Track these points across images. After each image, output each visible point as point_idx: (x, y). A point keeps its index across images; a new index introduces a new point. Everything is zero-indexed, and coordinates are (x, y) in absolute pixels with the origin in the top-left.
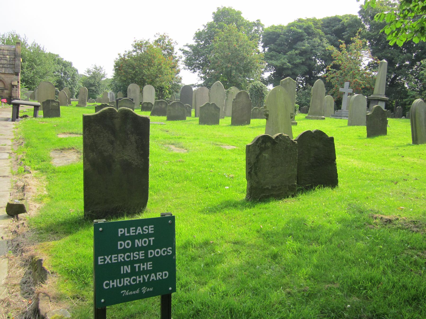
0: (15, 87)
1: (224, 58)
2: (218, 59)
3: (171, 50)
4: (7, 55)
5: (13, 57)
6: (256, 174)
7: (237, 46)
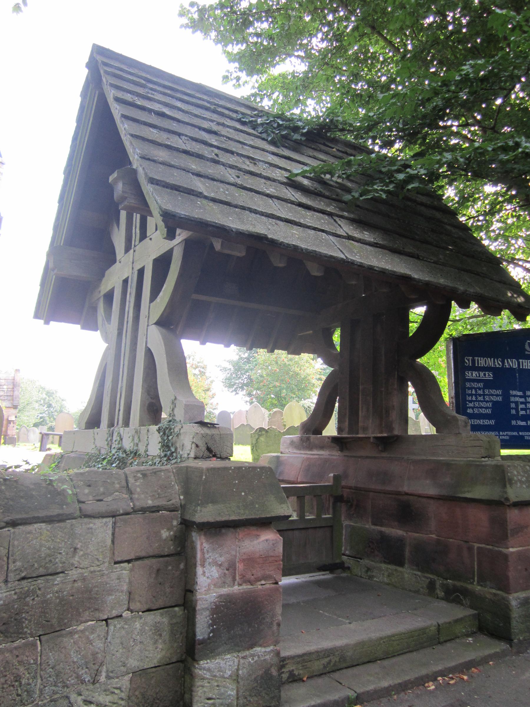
0: (12, 423)
1: (270, 375)
2: (264, 377)
3: (203, 368)
4: (4, 385)
5: (11, 387)
6: (257, 450)
7: (286, 360)
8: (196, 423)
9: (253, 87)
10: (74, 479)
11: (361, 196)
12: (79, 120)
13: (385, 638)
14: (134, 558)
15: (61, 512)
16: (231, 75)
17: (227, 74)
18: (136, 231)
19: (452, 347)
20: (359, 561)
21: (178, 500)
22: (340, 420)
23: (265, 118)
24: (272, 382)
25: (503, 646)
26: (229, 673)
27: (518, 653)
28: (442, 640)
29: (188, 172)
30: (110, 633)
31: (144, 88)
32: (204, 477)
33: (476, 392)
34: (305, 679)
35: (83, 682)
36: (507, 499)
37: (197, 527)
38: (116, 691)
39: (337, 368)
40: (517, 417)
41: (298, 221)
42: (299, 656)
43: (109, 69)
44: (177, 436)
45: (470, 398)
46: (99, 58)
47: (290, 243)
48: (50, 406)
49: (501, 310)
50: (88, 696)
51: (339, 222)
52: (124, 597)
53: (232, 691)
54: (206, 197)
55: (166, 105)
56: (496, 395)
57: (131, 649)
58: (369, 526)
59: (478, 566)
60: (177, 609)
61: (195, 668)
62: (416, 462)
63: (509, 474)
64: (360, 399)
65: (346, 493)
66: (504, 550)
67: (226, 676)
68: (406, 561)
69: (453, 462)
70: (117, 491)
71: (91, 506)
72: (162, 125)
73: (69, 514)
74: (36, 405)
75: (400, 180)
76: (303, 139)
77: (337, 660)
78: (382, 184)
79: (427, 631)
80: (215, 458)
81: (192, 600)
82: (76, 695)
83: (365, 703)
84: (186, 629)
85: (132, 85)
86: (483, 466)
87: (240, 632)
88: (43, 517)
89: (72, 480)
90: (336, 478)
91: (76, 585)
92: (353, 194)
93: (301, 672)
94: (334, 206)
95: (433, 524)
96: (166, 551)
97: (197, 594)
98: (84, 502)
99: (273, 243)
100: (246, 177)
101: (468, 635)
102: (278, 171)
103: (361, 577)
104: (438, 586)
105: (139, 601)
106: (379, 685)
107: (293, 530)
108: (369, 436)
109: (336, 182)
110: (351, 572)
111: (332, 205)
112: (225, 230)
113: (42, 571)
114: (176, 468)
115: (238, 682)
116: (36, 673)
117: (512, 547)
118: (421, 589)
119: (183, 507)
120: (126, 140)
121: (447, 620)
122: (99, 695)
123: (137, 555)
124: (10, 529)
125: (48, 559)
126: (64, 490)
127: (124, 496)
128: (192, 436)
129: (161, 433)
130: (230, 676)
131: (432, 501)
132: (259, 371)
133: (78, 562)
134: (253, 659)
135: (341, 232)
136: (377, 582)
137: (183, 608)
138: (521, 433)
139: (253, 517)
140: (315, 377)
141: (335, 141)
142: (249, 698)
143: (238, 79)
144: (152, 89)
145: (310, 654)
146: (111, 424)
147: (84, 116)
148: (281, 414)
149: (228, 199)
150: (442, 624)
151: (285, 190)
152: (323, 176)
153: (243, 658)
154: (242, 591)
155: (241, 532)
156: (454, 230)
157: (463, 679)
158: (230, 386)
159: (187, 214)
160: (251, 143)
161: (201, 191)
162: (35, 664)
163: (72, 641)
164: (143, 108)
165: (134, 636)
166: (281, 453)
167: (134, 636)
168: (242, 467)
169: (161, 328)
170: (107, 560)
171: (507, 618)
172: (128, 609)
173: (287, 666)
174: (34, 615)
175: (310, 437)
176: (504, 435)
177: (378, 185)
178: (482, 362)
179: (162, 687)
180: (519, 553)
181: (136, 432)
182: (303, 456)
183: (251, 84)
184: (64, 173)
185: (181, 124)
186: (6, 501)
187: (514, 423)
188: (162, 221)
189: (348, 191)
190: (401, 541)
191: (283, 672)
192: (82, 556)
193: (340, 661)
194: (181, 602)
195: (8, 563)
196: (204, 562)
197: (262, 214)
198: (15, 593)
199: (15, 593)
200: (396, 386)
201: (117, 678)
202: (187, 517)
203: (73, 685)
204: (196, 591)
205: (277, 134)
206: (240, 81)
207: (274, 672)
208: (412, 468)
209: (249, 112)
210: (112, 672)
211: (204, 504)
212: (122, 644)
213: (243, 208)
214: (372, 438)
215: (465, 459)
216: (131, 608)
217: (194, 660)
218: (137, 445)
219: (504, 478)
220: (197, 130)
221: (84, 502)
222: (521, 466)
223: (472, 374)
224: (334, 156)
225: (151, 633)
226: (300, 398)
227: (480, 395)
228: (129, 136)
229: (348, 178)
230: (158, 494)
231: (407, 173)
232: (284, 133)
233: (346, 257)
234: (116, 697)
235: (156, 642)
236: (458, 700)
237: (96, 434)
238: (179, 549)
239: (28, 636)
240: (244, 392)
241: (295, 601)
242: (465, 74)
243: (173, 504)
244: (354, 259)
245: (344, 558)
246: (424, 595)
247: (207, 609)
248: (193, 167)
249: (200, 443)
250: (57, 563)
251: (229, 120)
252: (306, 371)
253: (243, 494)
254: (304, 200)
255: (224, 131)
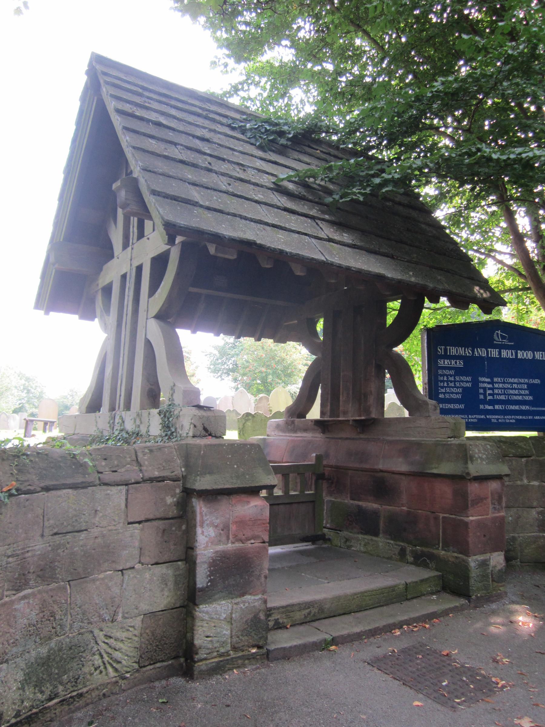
2: (249, 362)
6: (243, 434)
8: (193, 406)
9: (241, 74)
10: (93, 453)
11: (341, 198)
12: (79, 123)
13: (359, 593)
14: (144, 519)
15: (84, 480)
16: (219, 61)
17: (215, 59)
18: (134, 230)
19: (426, 337)
20: (338, 533)
21: (180, 472)
22: (323, 405)
23: (253, 123)
24: (258, 367)
25: (463, 601)
26: (224, 616)
27: (476, 607)
28: (409, 597)
29: (185, 181)
30: (125, 582)
31: (141, 96)
32: (202, 452)
33: (448, 378)
34: (288, 626)
35: (104, 620)
36: (468, 474)
37: (197, 494)
38: (131, 629)
39: (320, 355)
40: (484, 402)
41: (283, 225)
42: (283, 607)
43: (108, 79)
44: (177, 418)
45: (442, 384)
46: (99, 68)
47: (276, 247)
48: (29, 392)
49: (469, 305)
50: (108, 632)
51: (321, 225)
52: (136, 552)
53: (227, 631)
54: (201, 206)
55: (163, 113)
56: (466, 381)
57: (142, 595)
58: (348, 501)
59: (443, 533)
60: (180, 563)
61: (196, 611)
62: (390, 442)
63: (471, 452)
64: (341, 385)
65: (327, 471)
66: (466, 519)
67: (222, 618)
68: (381, 531)
69: (423, 442)
70: (129, 464)
71: (108, 476)
72: (160, 136)
73: (91, 482)
74: (15, 391)
75: (376, 184)
76: (289, 143)
77: (316, 611)
78: (360, 188)
79: (396, 588)
80: (210, 437)
81: (193, 556)
82: (98, 631)
83: (340, 645)
84: (187, 580)
85: (130, 94)
86: (448, 445)
87: (234, 583)
88: (70, 484)
89: (91, 454)
90: (318, 458)
91: (97, 541)
92: (334, 196)
93: (285, 620)
94: (317, 210)
95: (404, 498)
96: (170, 515)
97: (197, 550)
98: (101, 473)
99: (261, 247)
100: (236, 184)
101: (432, 593)
102: (265, 176)
103: (340, 547)
104: (408, 552)
105: (149, 556)
106: (352, 631)
107: (278, 504)
108: (348, 419)
109: (319, 185)
110: (331, 544)
111: (314, 208)
112: (220, 237)
113: (70, 528)
114: (177, 445)
115: (232, 624)
116: (67, 611)
117: (472, 516)
118: (393, 556)
119: (184, 478)
120: (129, 151)
121: (414, 580)
122: (117, 632)
123: (146, 517)
124: (44, 493)
125: (74, 519)
126: (86, 462)
127: (135, 468)
128: (190, 418)
129: (162, 416)
130: (225, 618)
131: (403, 477)
132: (245, 357)
133: (99, 522)
134: (244, 605)
135: (322, 235)
136: (355, 551)
137: (184, 562)
138: (488, 417)
139: (245, 486)
140: (301, 363)
141: (320, 142)
142: (241, 637)
143: (226, 65)
144: (148, 98)
145: (293, 605)
146: (112, 409)
147: (83, 120)
148: (268, 400)
149: (221, 207)
150: (410, 583)
151: (272, 196)
152: (307, 179)
153: (236, 604)
154: (235, 548)
155: (234, 499)
156: (428, 229)
157: (425, 627)
158: (215, 371)
159: (185, 224)
160: (241, 149)
161: (197, 201)
162: (66, 603)
163: (95, 587)
164: (141, 119)
165: (144, 584)
166: (268, 436)
167: (144, 584)
168: (234, 444)
169: (158, 321)
170: (122, 521)
171: (466, 578)
172: (139, 562)
173: (273, 615)
174: (64, 564)
175: (295, 420)
176: (472, 418)
177: (356, 188)
178: (453, 351)
179: (168, 627)
180: (478, 521)
181: (138, 415)
182: (288, 438)
183: (238, 71)
184: (64, 173)
185: (176, 132)
186: (40, 470)
187: (482, 407)
188: (164, 229)
189: (330, 193)
190: (376, 514)
191: (269, 621)
192: (102, 517)
193: (318, 613)
194: (183, 557)
195: (44, 521)
196: (203, 523)
197: (251, 220)
198: (50, 546)
199: (50, 546)
200: (373, 374)
201: (131, 618)
202: (188, 486)
203: (96, 622)
204: (196, 547)
205: (265, 139)
206: (228, 68)
207: (262, 616)
208: (387, 447)
209: (238, 116)
210: (127, 613)
211: (203, 474)
212: (135, 590)
213: (234, 215)
214: (351, 421)
215: (434, 439)
216: (142, 561)
217: (196, 605)
218: (139, 426)
219: (466, 455)
220: (191, 138)
221: (101, 473)
222: (482, 445)
223: (444, 362)
224: (318, 158)
225: (158, 582)
226: (286, 384)
227: (451, 382)
228: (131, 148)
229: (331, 180)
230: (163, 467)
231: (383, 177)
232: (271, 138)
233: (326, 259)
234: (130, 633)
235: (162, 590)
236: (419, 643)
237: (98, 417)
238: (181, 513)
239: (60, 581)
240: (230, 377)
241: (280, 566)
242: (436, 91)
243: (176, 475)
244: (334, 261)
245: (325, 530)
246: (396, 561)
247: (205, 562)
248: (190, 176)
249: (197, 424)
250: (81, 522)
251: (219, 126)
252: (292, 356)
253: (235, 466)
254: (290, 205)
255: (216, 138)
